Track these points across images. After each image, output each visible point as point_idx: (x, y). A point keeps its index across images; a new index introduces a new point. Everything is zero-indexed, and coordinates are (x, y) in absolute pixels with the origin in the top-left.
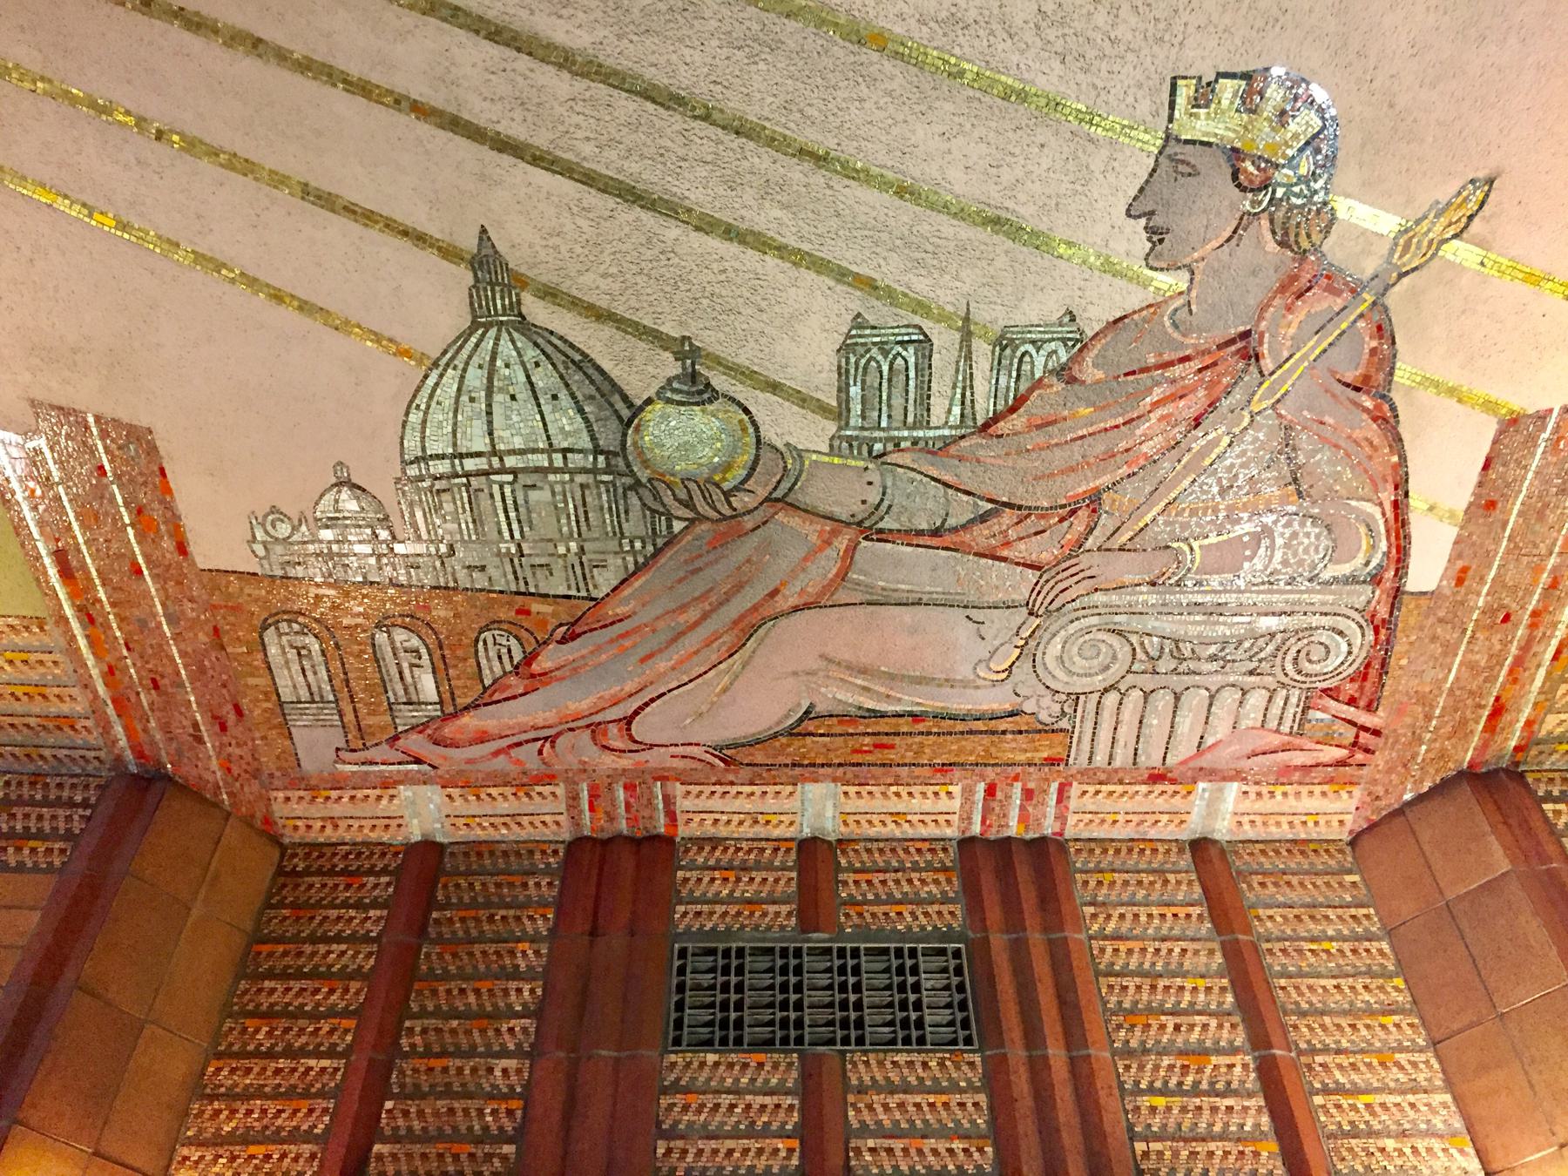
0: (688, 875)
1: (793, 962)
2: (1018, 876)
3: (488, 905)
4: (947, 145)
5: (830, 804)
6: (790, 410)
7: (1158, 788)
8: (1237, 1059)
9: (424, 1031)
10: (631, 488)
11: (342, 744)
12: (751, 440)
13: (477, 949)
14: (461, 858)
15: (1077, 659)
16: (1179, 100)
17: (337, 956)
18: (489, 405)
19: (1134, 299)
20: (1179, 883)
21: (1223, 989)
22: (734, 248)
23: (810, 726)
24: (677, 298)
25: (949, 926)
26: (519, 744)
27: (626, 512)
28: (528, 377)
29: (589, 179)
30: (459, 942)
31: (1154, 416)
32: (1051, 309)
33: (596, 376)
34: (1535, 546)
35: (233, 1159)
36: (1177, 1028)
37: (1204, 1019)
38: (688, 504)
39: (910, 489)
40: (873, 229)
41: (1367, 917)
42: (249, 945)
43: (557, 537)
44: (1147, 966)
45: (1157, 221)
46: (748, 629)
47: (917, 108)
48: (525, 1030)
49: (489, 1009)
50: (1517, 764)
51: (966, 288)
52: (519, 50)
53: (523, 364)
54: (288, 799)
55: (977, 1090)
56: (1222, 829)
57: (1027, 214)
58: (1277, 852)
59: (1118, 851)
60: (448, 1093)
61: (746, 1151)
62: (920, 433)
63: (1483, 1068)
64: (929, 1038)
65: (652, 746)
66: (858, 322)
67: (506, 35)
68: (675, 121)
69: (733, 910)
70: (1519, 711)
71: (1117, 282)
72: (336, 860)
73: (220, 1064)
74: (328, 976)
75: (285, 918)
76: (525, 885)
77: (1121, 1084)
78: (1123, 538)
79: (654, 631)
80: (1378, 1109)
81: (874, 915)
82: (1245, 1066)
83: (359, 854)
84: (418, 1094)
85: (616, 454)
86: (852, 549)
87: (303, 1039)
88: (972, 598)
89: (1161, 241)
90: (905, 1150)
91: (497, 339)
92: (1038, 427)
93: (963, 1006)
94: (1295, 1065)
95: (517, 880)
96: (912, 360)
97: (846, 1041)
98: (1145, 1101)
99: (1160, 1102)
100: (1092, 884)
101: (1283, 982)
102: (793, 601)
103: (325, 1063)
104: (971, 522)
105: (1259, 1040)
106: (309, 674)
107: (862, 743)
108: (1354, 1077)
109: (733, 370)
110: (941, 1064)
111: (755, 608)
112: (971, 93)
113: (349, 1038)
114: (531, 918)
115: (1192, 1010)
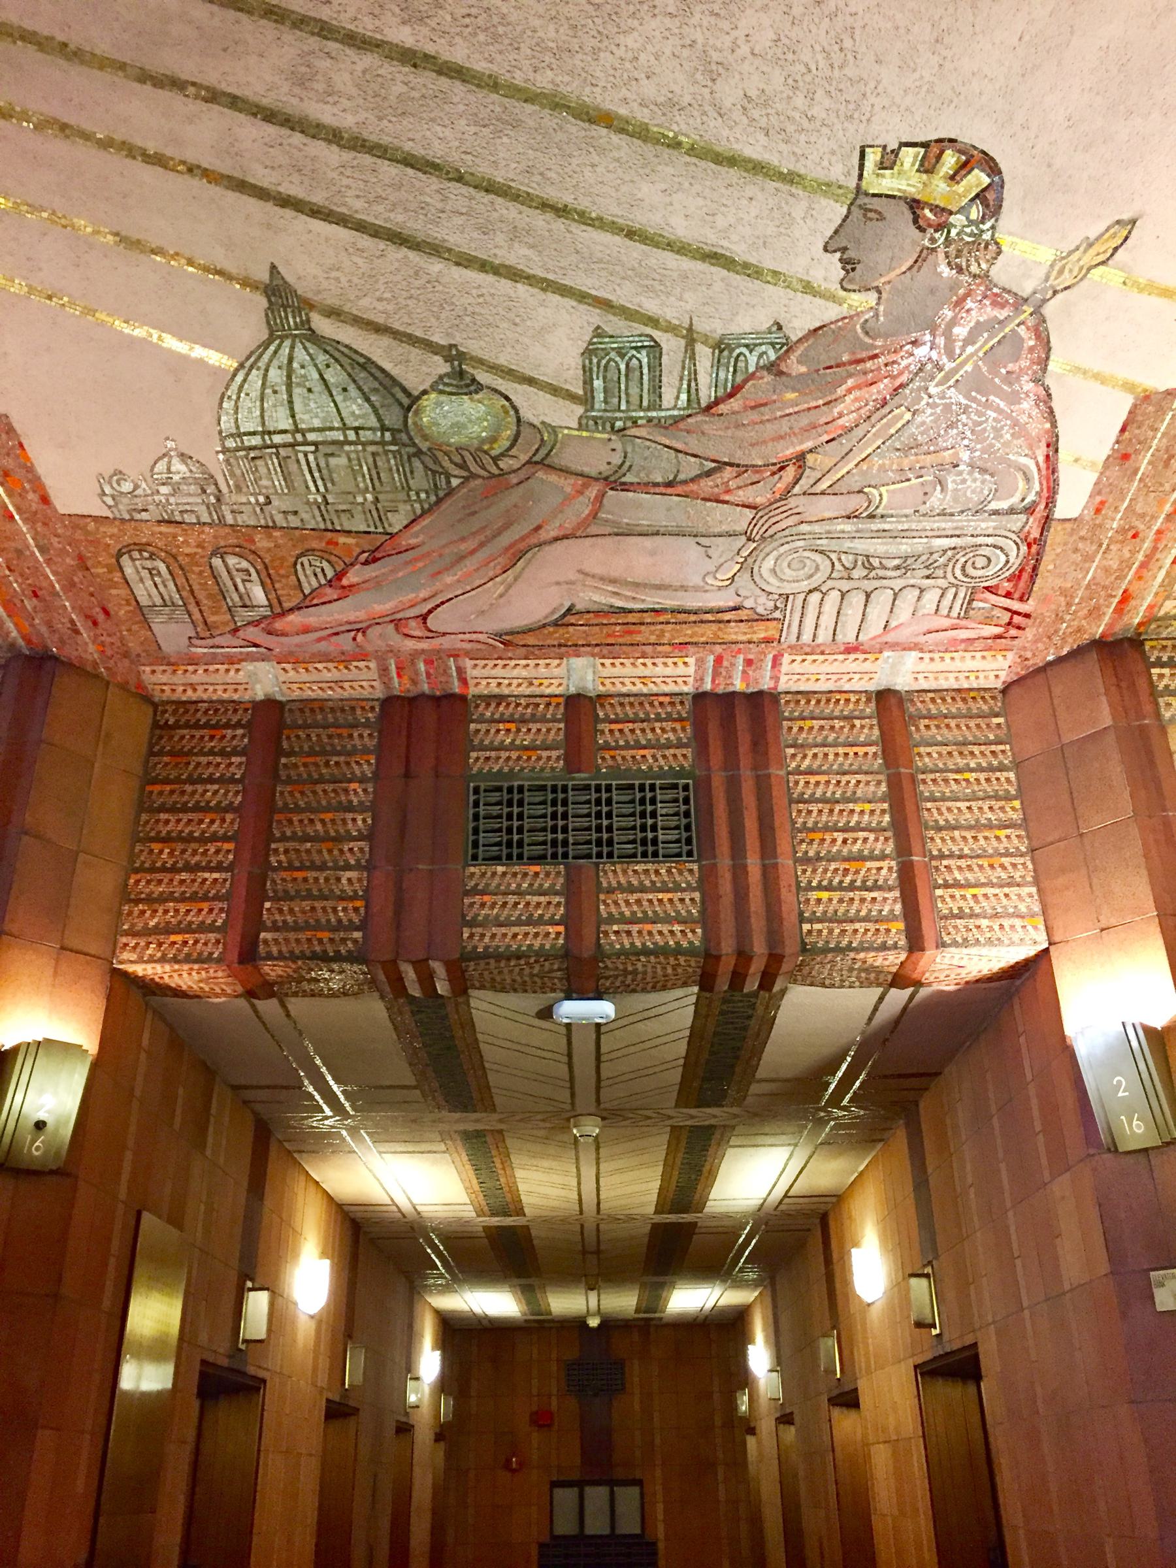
0: (479, 726)
1: (561, 796)
2: (738, 723)
3: (324, 753)
4: (668, 200)
5: (590, 671)
6: (545, 398)
7: (852, 656)
8: (885, 864)
9: (286, 851)
10: (415, 455)
11: (193, 634)
12: (512, 419)
13: (319, 788)
14: (298, 713)
15: (787, 570)
16: (867, 164)
17: (212, 793)
18: (290, 396)
19: (830, 312)
20: (863, 727)
21: (883, 812)
22: (490, 278)
23: (572, 619)
24: (443, 316)
25: (682, 766)
26: (337, 634)
27: (412, 472)
28: (321, 375)
29: (361, 227)
30: (304, 783)
31: (848, 399)
32: (764, 322)
33: (378, 374)
34: (1161, 485)
35: (160, 945)
36: (845, 841)
37: (865, 834)
38: (463, 466)
39: (647, 453)
40: (608, 262)
41: (1003, 752)
42: (142, 789)
43: (354, 490)
44: (829, 794)
45: (851, 254)
46: (517, 555)
47: (641, 171)
48: (361, 850)
49: (333, 834)
50: (1140, 634)
51: (688, 307)
52: (292, 129)
53: (316, 365)
54: (153, 672)
55: (694, 890)
56: (902, 682)
57: (739, 251)
58: (943, 700)
59: (818, 702)
60: (309, 896)
61: (526, 934)
62: (654, 414)
63: (1063, 871)
64: (661, 852)
65: (444, 634)
66: (598, 332)
67: (281, 118)
68: (433, 183)
69: (514, 755)
70: (1143, 599)
71: (818, 300)
72: (199, 715)
73: (138, 876)
74: (207, 809)
75: (167, 764)
76: (351, 736)
77: (798, 883)
78: (824, 485)
79: (441, 556)
80: (981, 898)
81: (624, 758)
82: (890, 869)
83: (216, 710)
84: (287, 897)
85: (400, 431)
86: (601, 496)
87: (197, 858)
88: (702, 530)
89: (853, 269)
90: (640, 932)
91: (292, 347)
92: (753, 408)
93: (688, 828)
94: (926, 866)
95: (345, 732)
96: (645, 361)
97: (599, 855)
98: (814, 895)
99: (825, 895)
100: (795, 730)
101: (929, 805)
102: (553, 534)
103: (216, 875)
104: (699, 477)
105: (903, 849)
106: (161, 587)
107: (616, 628)
108: (969, 875)
109: (494, 368)
110: (669, 871)
111: (523, 539)
112: (688, 159)
113: (231, 857)
114: (357, 763)
115: (858, 828)
